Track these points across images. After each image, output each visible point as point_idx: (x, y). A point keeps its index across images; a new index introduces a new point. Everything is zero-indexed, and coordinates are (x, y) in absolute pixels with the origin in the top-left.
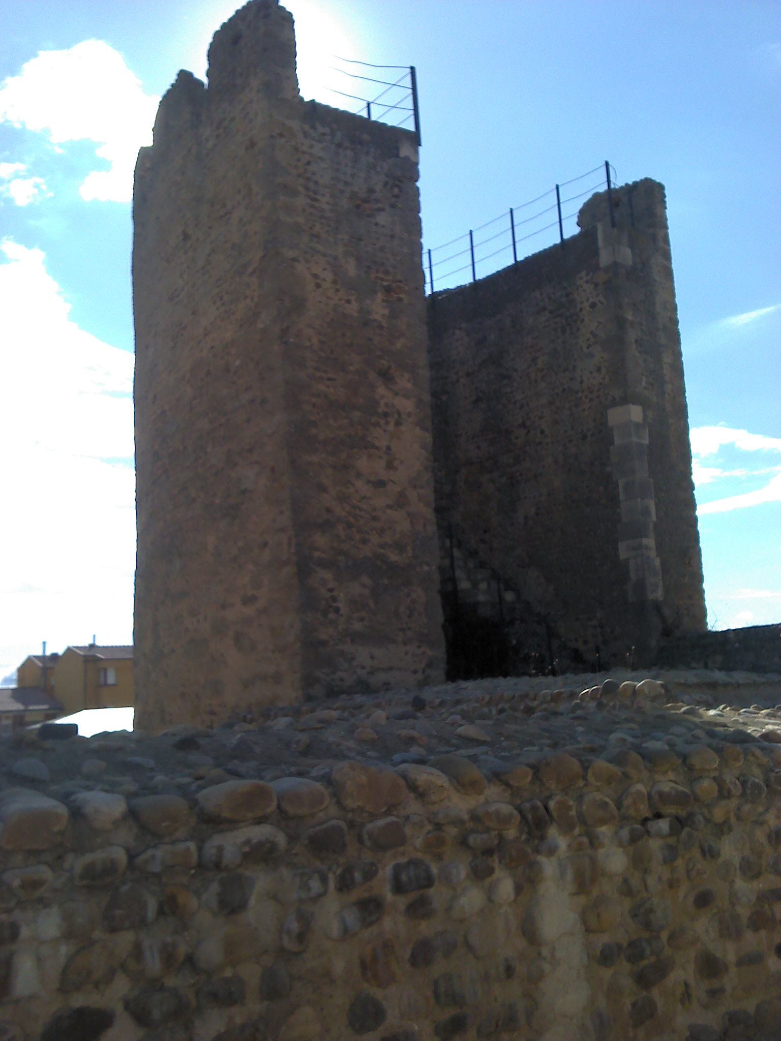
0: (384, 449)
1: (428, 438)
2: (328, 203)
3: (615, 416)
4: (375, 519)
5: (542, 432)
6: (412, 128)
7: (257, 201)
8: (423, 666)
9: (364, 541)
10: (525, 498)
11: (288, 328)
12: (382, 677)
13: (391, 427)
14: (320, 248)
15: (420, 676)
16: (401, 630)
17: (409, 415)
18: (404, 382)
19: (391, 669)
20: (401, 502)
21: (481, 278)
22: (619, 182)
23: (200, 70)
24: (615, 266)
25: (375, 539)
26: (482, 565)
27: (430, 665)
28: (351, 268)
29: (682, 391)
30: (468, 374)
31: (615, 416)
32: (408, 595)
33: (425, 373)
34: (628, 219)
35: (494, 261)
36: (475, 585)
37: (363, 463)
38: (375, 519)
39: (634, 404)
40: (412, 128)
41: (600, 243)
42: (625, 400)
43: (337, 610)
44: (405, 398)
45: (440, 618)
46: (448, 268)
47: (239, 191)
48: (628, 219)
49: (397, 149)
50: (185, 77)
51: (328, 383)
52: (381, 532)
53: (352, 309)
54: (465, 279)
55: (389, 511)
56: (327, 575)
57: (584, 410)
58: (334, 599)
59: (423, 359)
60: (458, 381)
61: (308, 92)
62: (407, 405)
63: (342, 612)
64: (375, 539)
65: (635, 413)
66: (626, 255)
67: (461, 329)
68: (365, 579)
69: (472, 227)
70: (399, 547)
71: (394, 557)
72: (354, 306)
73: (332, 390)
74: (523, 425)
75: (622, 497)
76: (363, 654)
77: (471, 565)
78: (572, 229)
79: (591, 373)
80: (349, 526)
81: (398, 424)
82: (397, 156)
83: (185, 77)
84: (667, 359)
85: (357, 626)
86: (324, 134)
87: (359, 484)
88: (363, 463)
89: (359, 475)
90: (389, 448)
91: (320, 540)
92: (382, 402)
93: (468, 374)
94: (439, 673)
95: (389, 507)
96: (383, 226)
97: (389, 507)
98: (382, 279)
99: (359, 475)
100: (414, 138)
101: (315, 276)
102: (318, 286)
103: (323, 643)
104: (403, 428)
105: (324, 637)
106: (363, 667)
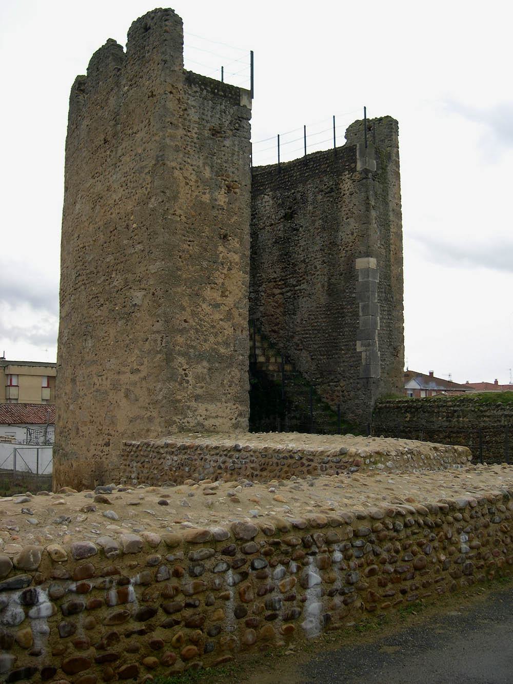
0: (221, 285)
1: (247, 278)
2: (196, 133)
3: (361, 263)
4: (213, 327)
5: (316, 267)
6: (249, 89)
7: (142, 104)
8: (236, 415)
9: (205, 341)
10: (302, 307)
11: (384, 597)
12: (212, 421)
13: (225, 271)
14: (189, 161)
15: (234, 421)
16: (225, 394)
17: (237, 264)
18: (234, 243)
19: (217, 417)
20: (229, 316)
21: (286, 161)
22: (370, 116)
23: (122, 41)
24: (366, 171)
25: (212, 339)
26: (272, 346)
27: (240, 415)
28: (207, 173)
29: (400, 249)
30: (272, 225)
31: (361, 263)
32: (230, 373)
33: (247, 238)
34: (375, 141)
35: (292, 153)
36: (268, 359)
37: (208, 293)
38: (213, 327)
39: (372, 257)
40: (249, 89)
41: (358, 157)
42: (368, 255)
43: (188, 382)
44: (235, 253)
45: (248, 387)
46: (263, 155)
47: (142, 122)
48: (375, 141)
49: (239, 101)
50: (111, 43)
51: (189, 243)
52: (216, 335)
53: (206, 198)
54: (274, 161)
55: (221, 322)
56: (181, 360)
57: (342, 257)
58: (186, 375)
59: (247, 229)
60: (264, 228)
61: (188, 66)
62: (236, 258)
63: (191, 382)
64: (212, 339)
65: (372, 262)
66: (373, 164)
67: (268, 195)
68: (205, 364)
69: (282, 133)
70: (226, 344)
71: (222, 350)
72: (208, 196)
73: (191, 248)
74: (304, 261)
75: (361, 314)
76: (202, 408)
77: (266, 346)
78: (341, 142)
79: (348, 235)
80: (197, 331)
81: (230, 269)
82: (239, 104)
83: (111, 43)
84: (393, 229)
85: (199, 391)
86: (197, 92)
87: (204, 306)
88: (208, 293)
89: (204, 300)
90: (223, 284)
91: (180, 339)
92: (221, 255)
93: (272, 225)
94: (245, 421)
95: (221, 320)
96: (228, 147)
97: (221, 320)
98: (225, 180)
99: (204, 300)
100: (250, 94)
101: (185, 178)
102: (187, 184)
103: (179, 401)
104: (232, 272)
105: (179, 397)
106: (201, 416)
